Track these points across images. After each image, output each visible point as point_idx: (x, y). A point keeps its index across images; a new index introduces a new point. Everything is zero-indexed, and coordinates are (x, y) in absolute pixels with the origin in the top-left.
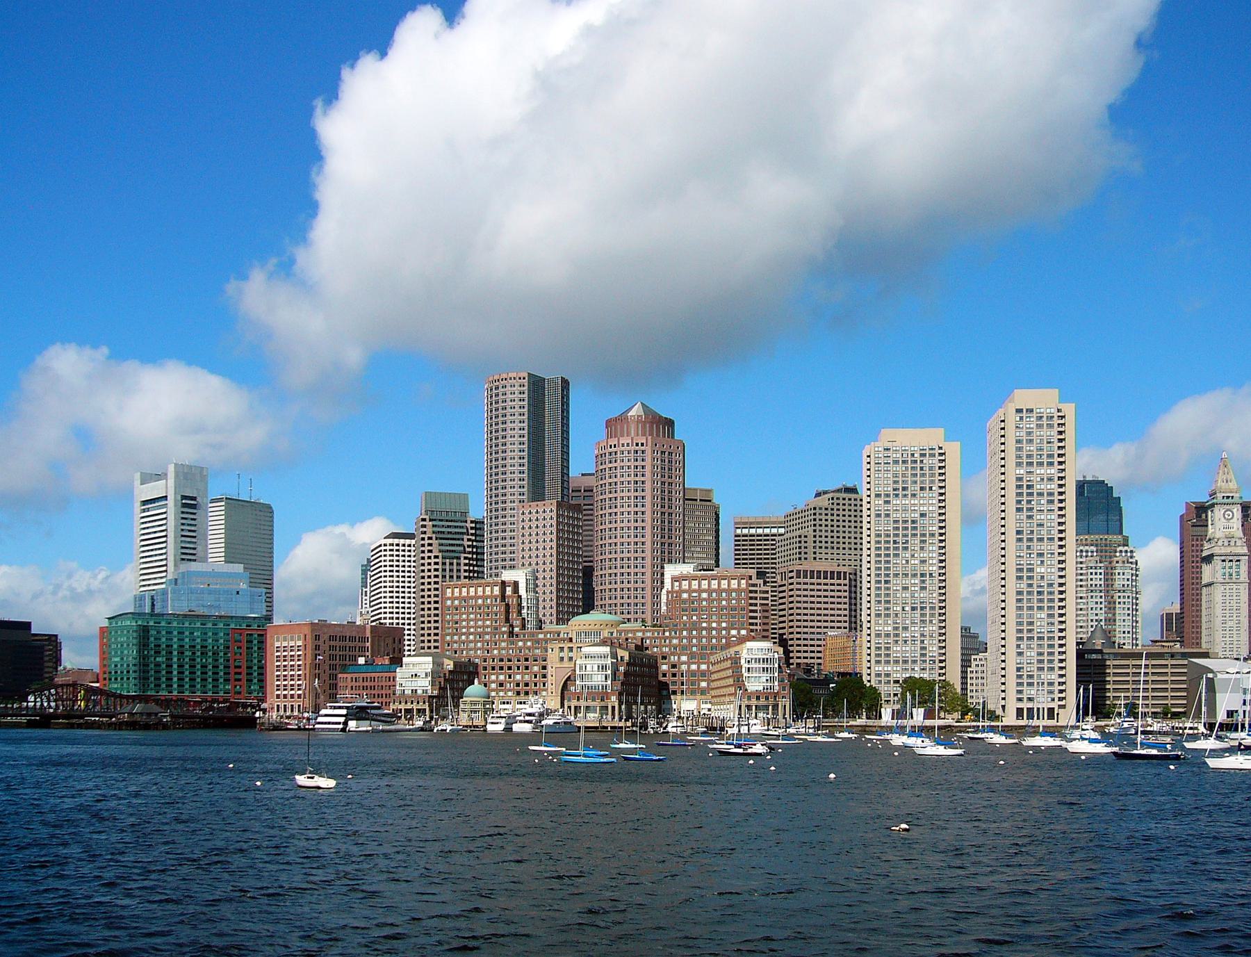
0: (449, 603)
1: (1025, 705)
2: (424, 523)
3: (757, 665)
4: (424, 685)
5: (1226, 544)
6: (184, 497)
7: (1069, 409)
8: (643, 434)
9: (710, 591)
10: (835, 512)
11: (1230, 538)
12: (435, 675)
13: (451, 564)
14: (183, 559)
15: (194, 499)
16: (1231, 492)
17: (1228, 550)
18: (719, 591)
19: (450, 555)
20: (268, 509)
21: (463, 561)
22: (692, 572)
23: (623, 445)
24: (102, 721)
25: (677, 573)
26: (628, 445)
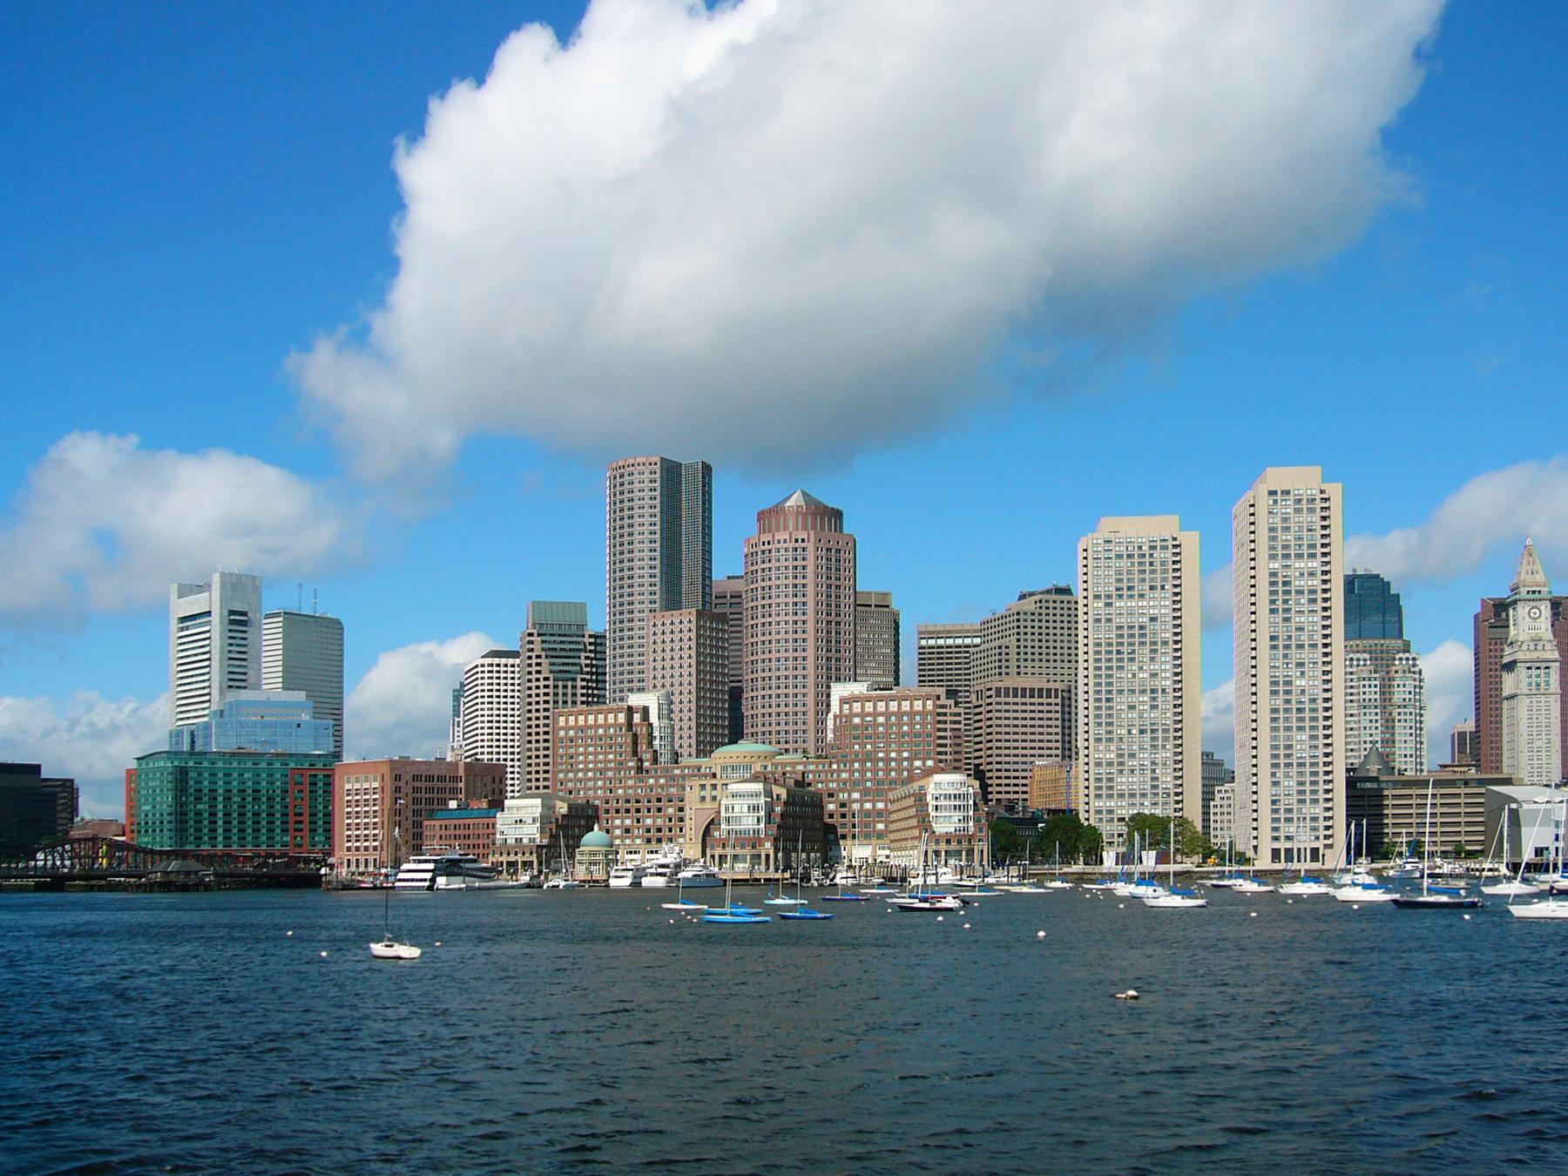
0: (562, 733)
1: (1283, 845)
4: (531, 832)
5: (1532, 647)
6: (232, 612)
7: (1335, 490)
8: (805, 528)
9: (887, 714)
11: (1537, 640)
12: (544, 820)
13: (565, 687)
14: (230, 687)
15: (244, 614)
16: (1538, 586)
17: (1535, 655)
18: (900, 714)
19: (563, 676)
20: (337, 625)
21: (580, 683)
22: (865, 692)
23: (779, 542)
25: (846, 694)
26: (785, 541)
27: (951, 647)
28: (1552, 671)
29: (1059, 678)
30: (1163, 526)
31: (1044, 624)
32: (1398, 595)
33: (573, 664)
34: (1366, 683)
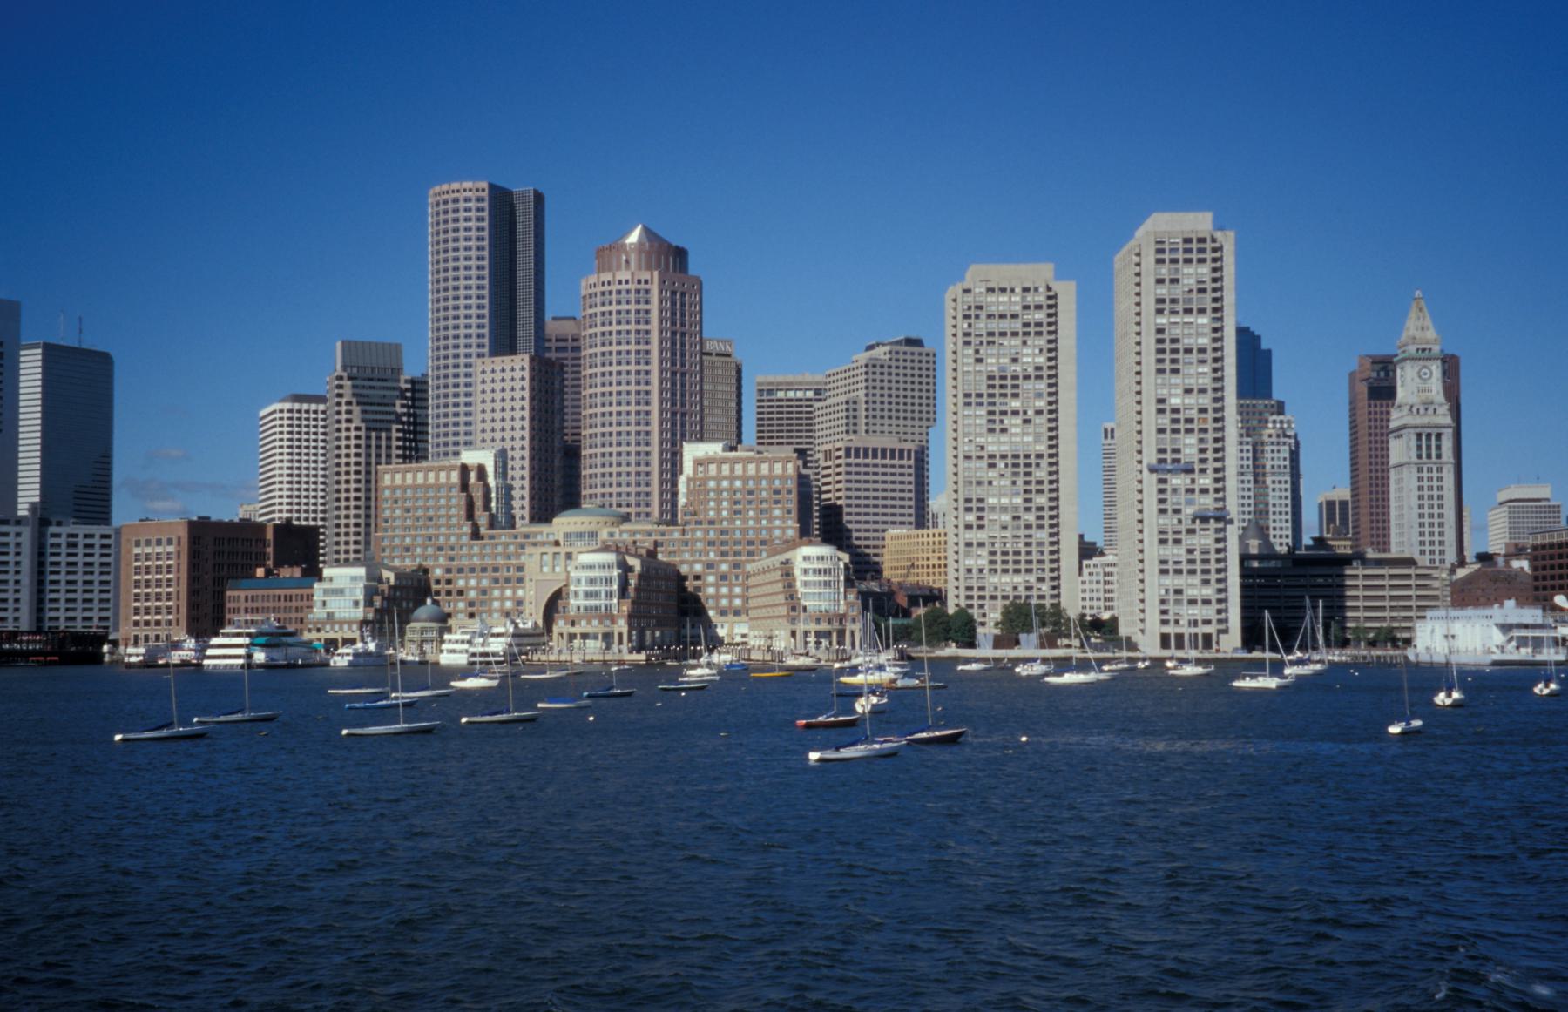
1: (1171, 630)
2: (341, 383)
3: (817, 578)
5: (1422, 411)
7: (1228, 240)
9: (745, 479)
10: (894, 371)
11: (1428, 404)
12: (370, 593)
13: (379, 438)
16: (1428, 343)
17: (1425, 420)
18: (758, 478)
19: (375, 426)
20: (104, 360)
21: (395, 435)
22: (720, 453)
23: (620, 282)
24: (637, 589)
27: (800, 400)
28: (1444, 438)
29: (909, 437)
30: (1040, 273)
31: (894, 378)
32: (1269, 352)
33: (386, 413)
34: (1275, 448)
